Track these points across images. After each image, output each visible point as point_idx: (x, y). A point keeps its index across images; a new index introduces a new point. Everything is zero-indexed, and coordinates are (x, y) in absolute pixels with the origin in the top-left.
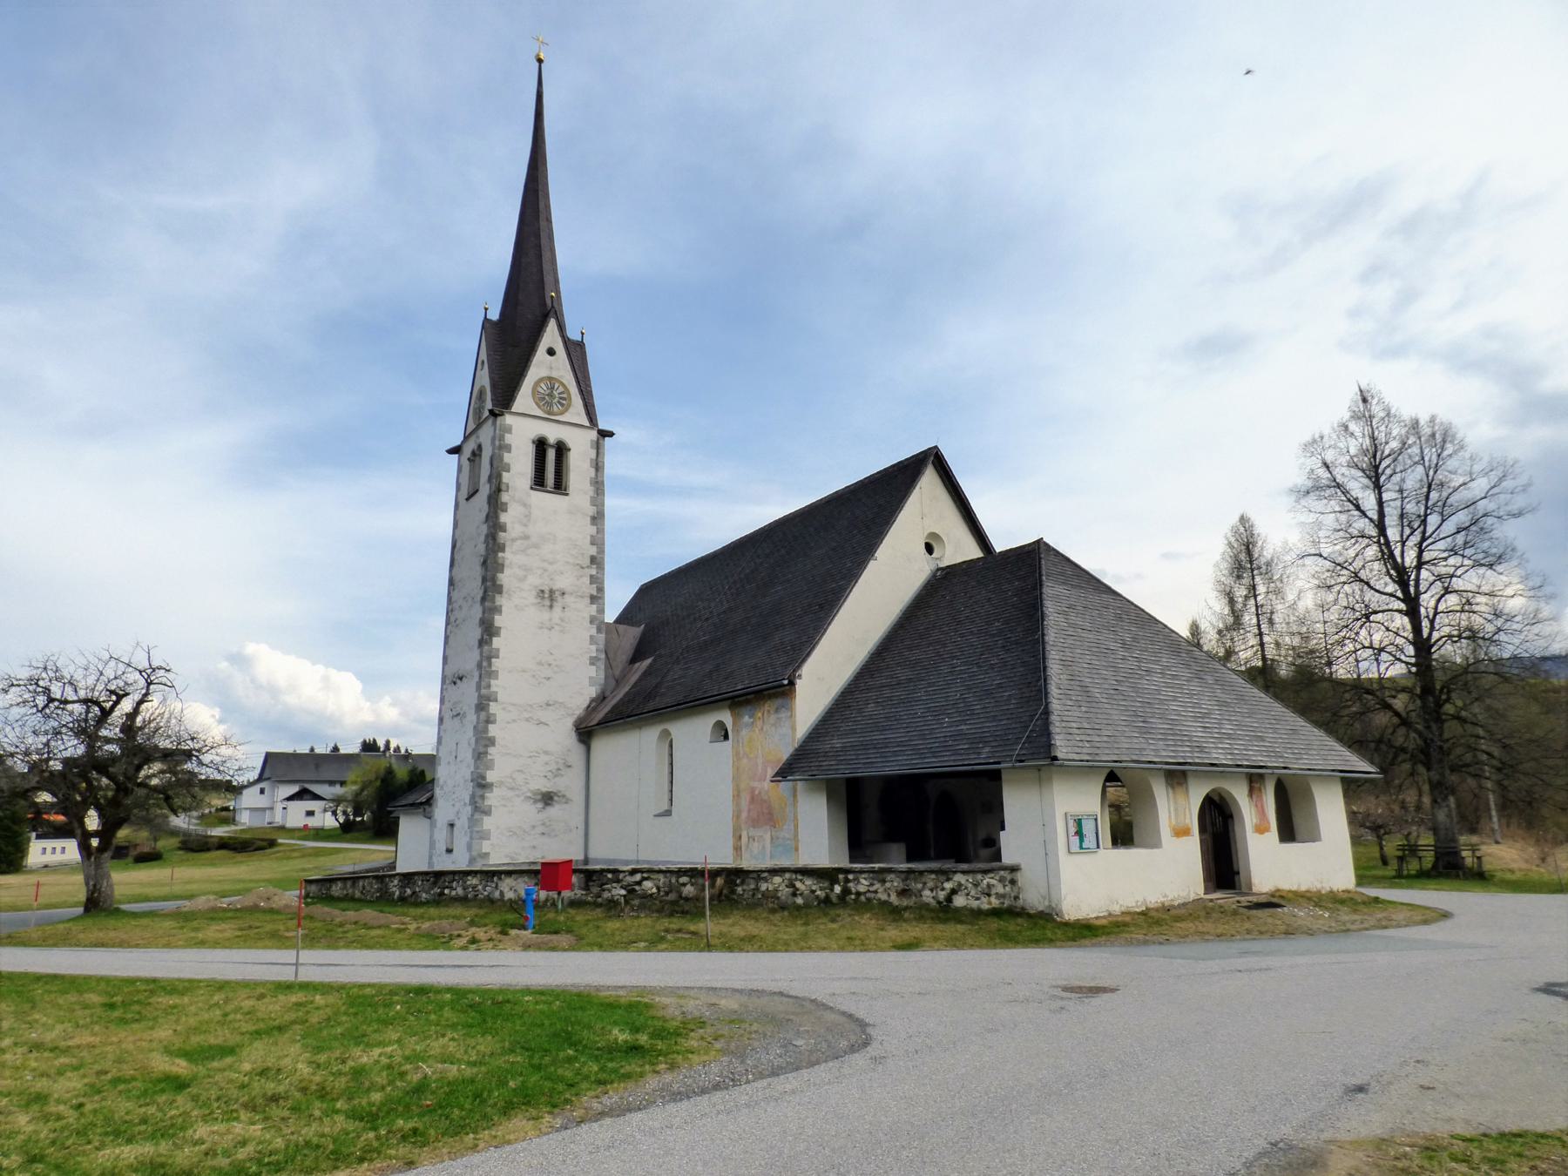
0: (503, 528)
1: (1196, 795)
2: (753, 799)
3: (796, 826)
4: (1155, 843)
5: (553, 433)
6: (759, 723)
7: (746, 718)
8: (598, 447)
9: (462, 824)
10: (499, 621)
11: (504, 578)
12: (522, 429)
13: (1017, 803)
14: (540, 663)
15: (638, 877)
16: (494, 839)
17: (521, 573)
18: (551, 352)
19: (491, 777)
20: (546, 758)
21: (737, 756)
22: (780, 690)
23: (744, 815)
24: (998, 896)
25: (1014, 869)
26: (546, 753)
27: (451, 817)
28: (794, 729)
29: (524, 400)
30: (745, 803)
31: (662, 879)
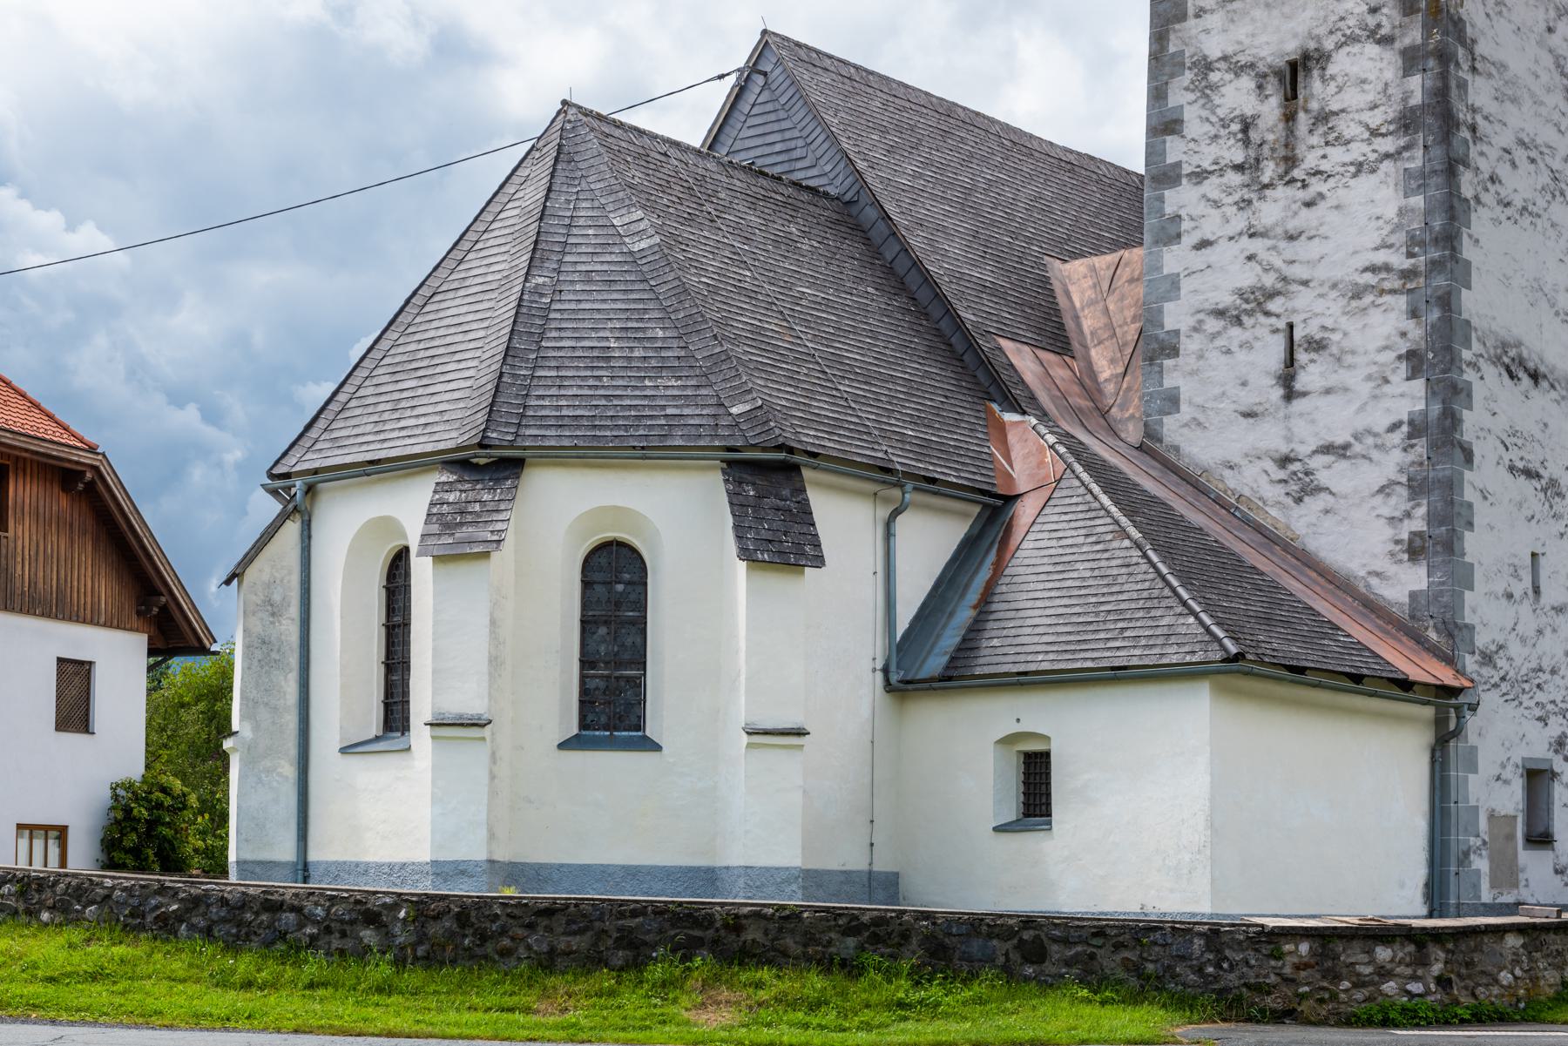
27: (1537, 745)
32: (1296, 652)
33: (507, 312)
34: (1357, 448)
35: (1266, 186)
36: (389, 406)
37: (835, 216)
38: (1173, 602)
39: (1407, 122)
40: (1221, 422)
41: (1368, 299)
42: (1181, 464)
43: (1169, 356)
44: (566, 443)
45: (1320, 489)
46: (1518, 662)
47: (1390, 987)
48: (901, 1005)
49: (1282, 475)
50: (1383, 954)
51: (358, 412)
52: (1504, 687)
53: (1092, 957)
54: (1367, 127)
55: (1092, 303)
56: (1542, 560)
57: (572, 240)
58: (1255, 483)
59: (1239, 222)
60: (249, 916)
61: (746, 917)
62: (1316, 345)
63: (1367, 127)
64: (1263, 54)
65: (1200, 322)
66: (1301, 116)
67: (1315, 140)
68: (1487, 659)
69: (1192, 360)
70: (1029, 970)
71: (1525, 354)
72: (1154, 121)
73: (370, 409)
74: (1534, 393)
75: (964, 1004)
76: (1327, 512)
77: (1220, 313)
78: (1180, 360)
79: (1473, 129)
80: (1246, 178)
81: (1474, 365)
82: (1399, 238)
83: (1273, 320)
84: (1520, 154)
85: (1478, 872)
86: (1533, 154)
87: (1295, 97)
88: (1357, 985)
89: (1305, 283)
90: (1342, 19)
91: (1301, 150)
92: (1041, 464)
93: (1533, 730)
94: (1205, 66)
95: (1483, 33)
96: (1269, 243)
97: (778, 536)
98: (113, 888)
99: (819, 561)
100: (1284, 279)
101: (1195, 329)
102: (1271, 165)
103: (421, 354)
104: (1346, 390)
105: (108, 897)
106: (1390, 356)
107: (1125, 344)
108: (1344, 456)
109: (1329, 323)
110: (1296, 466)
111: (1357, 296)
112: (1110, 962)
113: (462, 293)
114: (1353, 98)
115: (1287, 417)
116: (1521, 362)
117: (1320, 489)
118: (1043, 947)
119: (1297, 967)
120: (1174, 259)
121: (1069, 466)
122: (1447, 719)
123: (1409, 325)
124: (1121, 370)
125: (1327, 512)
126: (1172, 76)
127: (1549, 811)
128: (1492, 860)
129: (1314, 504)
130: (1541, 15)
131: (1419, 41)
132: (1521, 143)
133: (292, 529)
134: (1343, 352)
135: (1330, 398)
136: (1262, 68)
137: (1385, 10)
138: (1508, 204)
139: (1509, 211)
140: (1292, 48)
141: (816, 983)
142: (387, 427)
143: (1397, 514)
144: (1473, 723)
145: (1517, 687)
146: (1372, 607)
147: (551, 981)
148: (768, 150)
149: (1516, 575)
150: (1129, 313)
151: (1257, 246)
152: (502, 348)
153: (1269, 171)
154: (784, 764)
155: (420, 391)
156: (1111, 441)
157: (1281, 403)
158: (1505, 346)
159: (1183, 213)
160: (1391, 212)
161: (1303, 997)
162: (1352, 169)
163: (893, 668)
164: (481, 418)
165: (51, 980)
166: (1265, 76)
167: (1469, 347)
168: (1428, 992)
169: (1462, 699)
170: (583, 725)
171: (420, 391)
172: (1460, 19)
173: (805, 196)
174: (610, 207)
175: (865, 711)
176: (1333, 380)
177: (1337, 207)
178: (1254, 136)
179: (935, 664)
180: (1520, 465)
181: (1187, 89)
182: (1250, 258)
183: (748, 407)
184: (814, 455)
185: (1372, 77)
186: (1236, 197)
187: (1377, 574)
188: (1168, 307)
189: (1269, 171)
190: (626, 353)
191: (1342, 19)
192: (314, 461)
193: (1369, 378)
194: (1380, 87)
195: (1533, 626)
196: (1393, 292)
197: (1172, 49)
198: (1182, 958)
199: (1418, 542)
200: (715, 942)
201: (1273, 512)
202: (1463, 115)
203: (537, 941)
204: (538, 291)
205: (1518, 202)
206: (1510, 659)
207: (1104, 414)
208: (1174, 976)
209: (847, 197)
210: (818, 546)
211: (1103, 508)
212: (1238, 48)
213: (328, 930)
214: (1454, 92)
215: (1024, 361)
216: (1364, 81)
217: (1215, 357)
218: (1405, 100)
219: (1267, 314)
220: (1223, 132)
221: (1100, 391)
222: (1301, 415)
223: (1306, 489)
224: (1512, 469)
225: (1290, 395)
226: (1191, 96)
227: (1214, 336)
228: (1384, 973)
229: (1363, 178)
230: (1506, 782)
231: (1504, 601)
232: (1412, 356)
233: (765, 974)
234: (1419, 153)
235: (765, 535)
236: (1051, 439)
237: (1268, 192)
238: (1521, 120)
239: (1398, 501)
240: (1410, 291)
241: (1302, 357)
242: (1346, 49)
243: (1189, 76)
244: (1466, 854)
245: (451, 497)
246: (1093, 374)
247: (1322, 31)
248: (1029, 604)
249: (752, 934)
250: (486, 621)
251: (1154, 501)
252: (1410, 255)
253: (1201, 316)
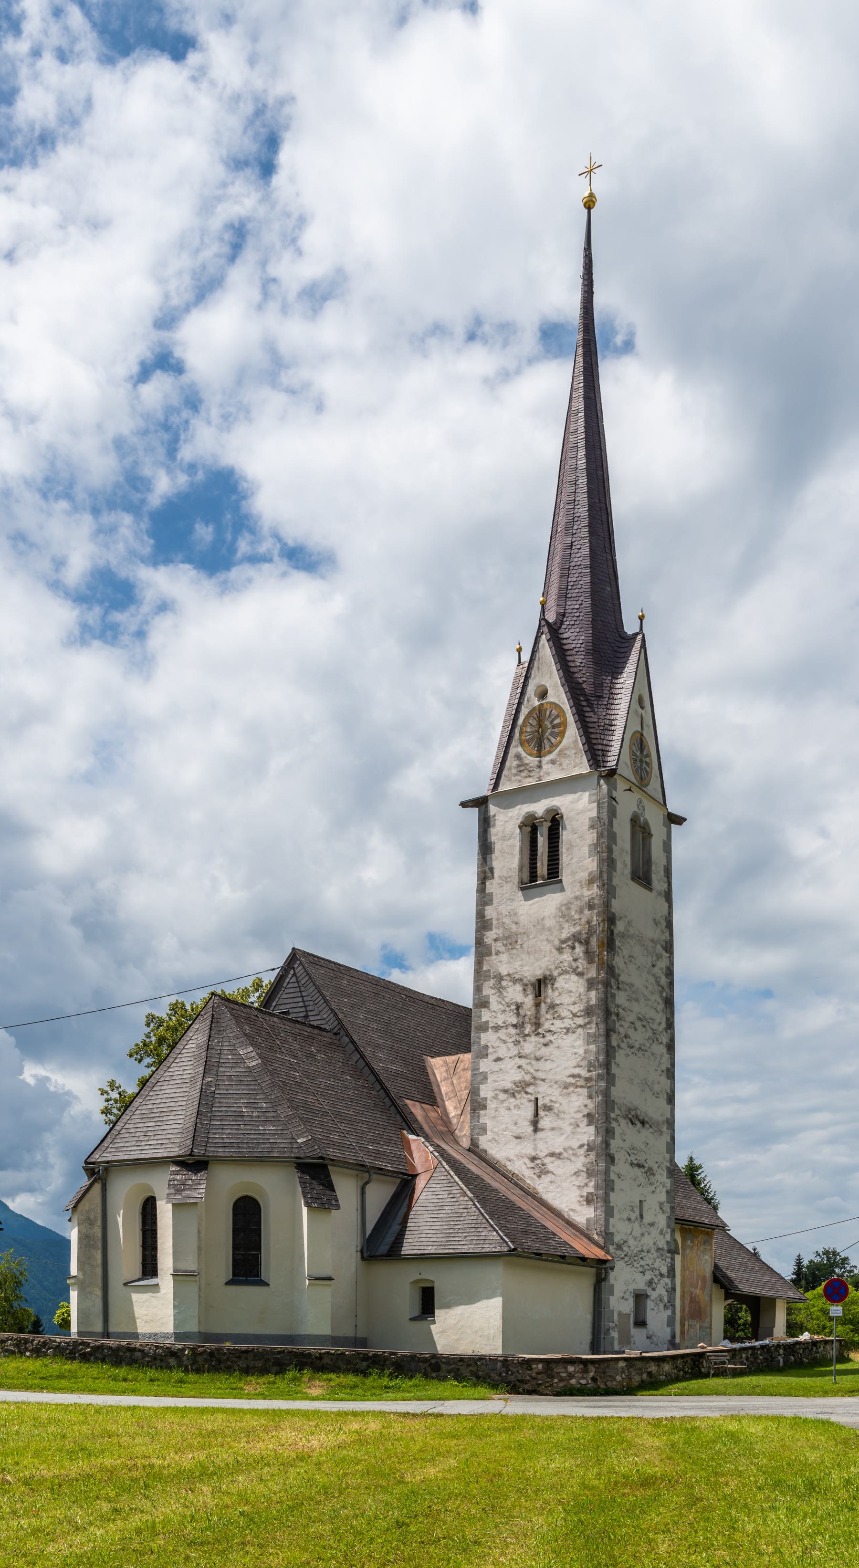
2: (691, 1301)
27: (640, 1283)
30: (687, 1302)
32: (539, 1247)
33: (196, 1093)
34: (565, 1155)
35: (526, 1035)
36: (142, 1134)
37: (330, 1040)
38: (487, 1225)
39: (588, 1012)
40: (505, 1139)
41: (571, 1089)
42: (487, 1158)
43: (482, 1109)
44: (227, 1154)
45: (548, 1172)
46: (632, 1248)
47: (573, 1381)
48: (386, 1387)
49: (532, 1165)
50: (571, 1369)
51: (127, 1135)
52: (626, 1259)
53: (458, 1369)
54: (572, 1012)
55: (446, 1079)
56: (644, 1204)
57: (222, 1061)
58: (521, 1168)
59: (514, 1051)
60: (121, 1354)
61: (324, 1354)
62: (548, 1108)
63: (572, 1012)
64: (526, 975)
65: (497, 1095)
66: (543, 1005)
67: (549, 1016)
68: (619, 1247)
69: (493, 1112)
70: (434, 1375)
71: (639, 1113)
72: (476, 1001)
73: (133, 1135)
74: (643, 1130)
75: (411, 1387)
76: (551, 1182)
77: (505, 1091)
78: (487, 1111)
79: (617, 1015)
80: (518, 1031)
81: (616, 1120)
82: (584, 1063)
83: (529, 1096)
84: (638, 1024)
85: (613, 1338)
86: (645, 1023)
87: (540, 995)
88: (560, 1381)
89: (543, 1080)
90: (561, 962)
91: (542, 1020)
92: (427, 1160)
93: (639, 1277)
94: (500, 978)
95: (623, 971)
96: (528, 1061)
97: (322, 1197)
98: (61, 1342)
99: (338, 1207)
100: (534, 1078)
101: (494, 1098)
102: (529, 1026)
103: (155, 1110)
104: (561, 1129)
105: (58, 1346)
106: (580, 1115)
107: (461, 1100)
108: (559, 1158)
109: (554, 1099)
110: (538, 1162)
111: (566, 1087)
112: (464, 1371)
113: (172, 1082)
114: (566, 999)
115: (535, 1140)
116: (637, 1117)
117: (548, 1172)
118: (439, 1365)
119: (538, 1373)
120: (485, 1065)
121: (440, 1162)
122: (601, 1273)
123: (589, 1102)
124: (460, 1112)
125: (551, 1182)
126: (485, 981)
127: (645, 1312)
128: (619, 1333)
129: (546, 1179)
130: (649, 959)
131: (594, 975)
132: (639, 1019)
133: (97, 1187)
134: (559, 1111)
135: (553, 1132)
136: (525, 981)
137: (580, 960)
138: (632, 1047)
139: (633, 1050)
140: (539, 973)
141: (351, 1379)
142: (143, 1143)
143: (582, 1184)
144: (612, 1275)
145: (631, 1259)
146: (570, 1224)
147: (250, 1378)
148: (295, 1005)
149: (632, 1210)
150: (463, 1085)
151: (522, 1062)
152: (196, 1111)
153: (528, 1029)
154: (325, 1292)
155: (157, 1128)
156: (456, 1147)
157: (532, 1133)
158: (630, 1110)
159: (489, 1045)
160: (581, 1051)
161: (540, 1385)
162: (565, 1031)
163: (365, 1250)
164: (189, 1142)
165: (43, 1378)
166: (527, 985)
167: (614, 1112)
168: (588, 1383)
169: (608, 1265)
170: (234, 1275)
171: (157, 1128)
172: (613, 967)
173: (316, 1031)
174: (238, 1045)
175: (353, 1269)
176: (555, 1124)
177: (558, 1047)
178: (521, 1011)
179: (384, 1249)
180: (635, 1162)
181: (491, 988)
182: (519, 1067)
183: (305, 1140)
184: (333, 1160)
185: (574, 990)
186: (513, 1039)
187: (573, 1210)
188: (482, 1087)
189: (528, 1029)
190: (250, 1114)
191: (561, 962)
192: (107, 1157)
193: (571, 1124)
194: (577, 995)
195: (640, 1232)
196: (581, 1087)
197: (485, 969)
198: (493, 1370)
199: (590, 1197)
200: (312, 1363)
201: (528, 1182)
202: (613, 1009)
203: (242, 1364)
204: (209, 1085)
205: (637, 1045)
206: (629, 1247)
207: (452, 1133)
208: (490, 1377)
209: (335, 1031)
210: (337, 1200)
211: (455, 1182)
212: (514, 971)
213: (155, 1359)
214: (609, 999)
215: (417, 1110)
216: (570, 992)
217: (503, 1111)
218: (588, 1002)
219: (527, 1093)
220: (507, 1009)
221: (450, 1122)
222: (541, 1139)
223: (543, 1172)
224: (632, 1164)
225: (536, 1130)
226: (493, 991)
227: (503, 1101)
228: (571, 1376)
229: (570, 1034)
230: (627, 1299)
231: (627, 1222)
232: (589, 1116)
233: (333, 1376)
234: (594, 1026)
235: (315, 1196)
236: (431, 1149)
237: (527, 1038)
238: (639, 1008)
239: (582, 1179)
240: (589, 1087)
241: (541, 1113)
242: (563, 976)
243: (492, 982)
244: (608, 1330)
245: (178, 1177)
246: (446, 1113)
247: (553, 967)
248: (424, 1224)
249: (327, 1360)
250: (196, 1231)
251: (478, 1177)
252: (589, 1071)
253: (497, 1092)
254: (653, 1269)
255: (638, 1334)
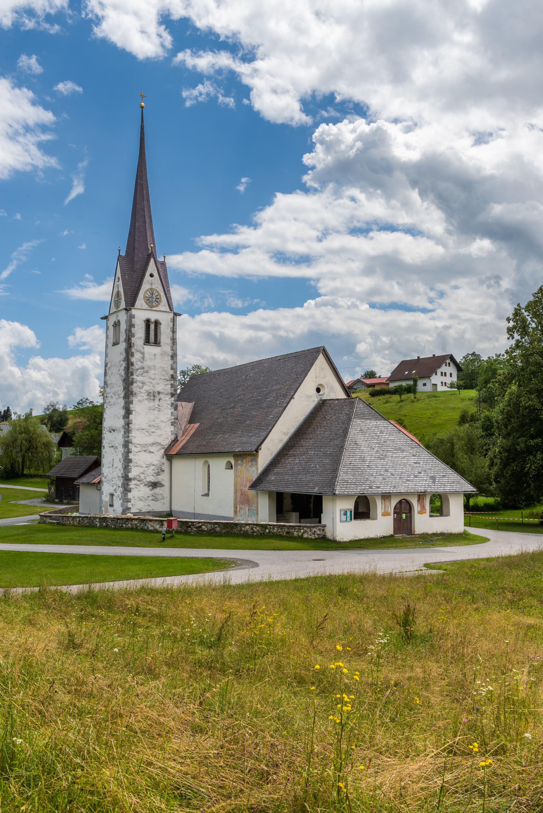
0: (132, 364)
1: (394, 502)
2: (242, 494)
3: (257, 506)
4: (376, 519)
5: (153, 316)
6: (245, 465)
7: (240, 462)
8: (174, 321)
9: (119, 493)
10: (132, 407)
11: (135, 388)
12: (141, 314)
13: (327, 505)
14: (150, 426)
15: (200, 524)
16: (132, 502)
17: (141, 385)
18: (152, 275)
19: (131, 475)
20: (153, 467)
21: (236, 476)
22: (253, 454)
23: (238, 499)
24: (318, 534)
25: (325, 526)
26: (153, 465)
27: (112, 491)
28: (257, 469)
29: (140, 302)
30: (239, 494)
31: (209, 526)
145: (109, 482)
254: (116, 485)
255: (110, 509)
